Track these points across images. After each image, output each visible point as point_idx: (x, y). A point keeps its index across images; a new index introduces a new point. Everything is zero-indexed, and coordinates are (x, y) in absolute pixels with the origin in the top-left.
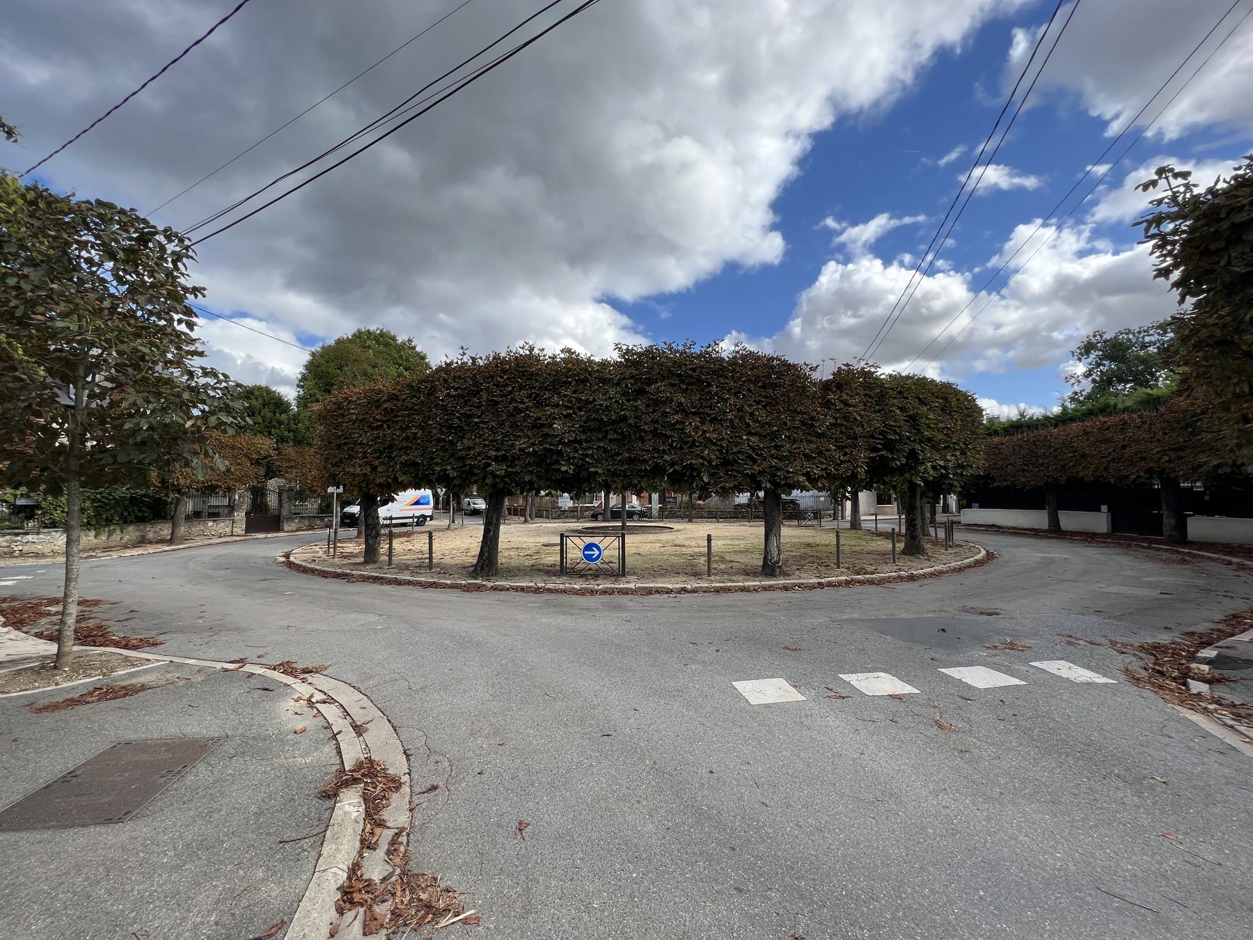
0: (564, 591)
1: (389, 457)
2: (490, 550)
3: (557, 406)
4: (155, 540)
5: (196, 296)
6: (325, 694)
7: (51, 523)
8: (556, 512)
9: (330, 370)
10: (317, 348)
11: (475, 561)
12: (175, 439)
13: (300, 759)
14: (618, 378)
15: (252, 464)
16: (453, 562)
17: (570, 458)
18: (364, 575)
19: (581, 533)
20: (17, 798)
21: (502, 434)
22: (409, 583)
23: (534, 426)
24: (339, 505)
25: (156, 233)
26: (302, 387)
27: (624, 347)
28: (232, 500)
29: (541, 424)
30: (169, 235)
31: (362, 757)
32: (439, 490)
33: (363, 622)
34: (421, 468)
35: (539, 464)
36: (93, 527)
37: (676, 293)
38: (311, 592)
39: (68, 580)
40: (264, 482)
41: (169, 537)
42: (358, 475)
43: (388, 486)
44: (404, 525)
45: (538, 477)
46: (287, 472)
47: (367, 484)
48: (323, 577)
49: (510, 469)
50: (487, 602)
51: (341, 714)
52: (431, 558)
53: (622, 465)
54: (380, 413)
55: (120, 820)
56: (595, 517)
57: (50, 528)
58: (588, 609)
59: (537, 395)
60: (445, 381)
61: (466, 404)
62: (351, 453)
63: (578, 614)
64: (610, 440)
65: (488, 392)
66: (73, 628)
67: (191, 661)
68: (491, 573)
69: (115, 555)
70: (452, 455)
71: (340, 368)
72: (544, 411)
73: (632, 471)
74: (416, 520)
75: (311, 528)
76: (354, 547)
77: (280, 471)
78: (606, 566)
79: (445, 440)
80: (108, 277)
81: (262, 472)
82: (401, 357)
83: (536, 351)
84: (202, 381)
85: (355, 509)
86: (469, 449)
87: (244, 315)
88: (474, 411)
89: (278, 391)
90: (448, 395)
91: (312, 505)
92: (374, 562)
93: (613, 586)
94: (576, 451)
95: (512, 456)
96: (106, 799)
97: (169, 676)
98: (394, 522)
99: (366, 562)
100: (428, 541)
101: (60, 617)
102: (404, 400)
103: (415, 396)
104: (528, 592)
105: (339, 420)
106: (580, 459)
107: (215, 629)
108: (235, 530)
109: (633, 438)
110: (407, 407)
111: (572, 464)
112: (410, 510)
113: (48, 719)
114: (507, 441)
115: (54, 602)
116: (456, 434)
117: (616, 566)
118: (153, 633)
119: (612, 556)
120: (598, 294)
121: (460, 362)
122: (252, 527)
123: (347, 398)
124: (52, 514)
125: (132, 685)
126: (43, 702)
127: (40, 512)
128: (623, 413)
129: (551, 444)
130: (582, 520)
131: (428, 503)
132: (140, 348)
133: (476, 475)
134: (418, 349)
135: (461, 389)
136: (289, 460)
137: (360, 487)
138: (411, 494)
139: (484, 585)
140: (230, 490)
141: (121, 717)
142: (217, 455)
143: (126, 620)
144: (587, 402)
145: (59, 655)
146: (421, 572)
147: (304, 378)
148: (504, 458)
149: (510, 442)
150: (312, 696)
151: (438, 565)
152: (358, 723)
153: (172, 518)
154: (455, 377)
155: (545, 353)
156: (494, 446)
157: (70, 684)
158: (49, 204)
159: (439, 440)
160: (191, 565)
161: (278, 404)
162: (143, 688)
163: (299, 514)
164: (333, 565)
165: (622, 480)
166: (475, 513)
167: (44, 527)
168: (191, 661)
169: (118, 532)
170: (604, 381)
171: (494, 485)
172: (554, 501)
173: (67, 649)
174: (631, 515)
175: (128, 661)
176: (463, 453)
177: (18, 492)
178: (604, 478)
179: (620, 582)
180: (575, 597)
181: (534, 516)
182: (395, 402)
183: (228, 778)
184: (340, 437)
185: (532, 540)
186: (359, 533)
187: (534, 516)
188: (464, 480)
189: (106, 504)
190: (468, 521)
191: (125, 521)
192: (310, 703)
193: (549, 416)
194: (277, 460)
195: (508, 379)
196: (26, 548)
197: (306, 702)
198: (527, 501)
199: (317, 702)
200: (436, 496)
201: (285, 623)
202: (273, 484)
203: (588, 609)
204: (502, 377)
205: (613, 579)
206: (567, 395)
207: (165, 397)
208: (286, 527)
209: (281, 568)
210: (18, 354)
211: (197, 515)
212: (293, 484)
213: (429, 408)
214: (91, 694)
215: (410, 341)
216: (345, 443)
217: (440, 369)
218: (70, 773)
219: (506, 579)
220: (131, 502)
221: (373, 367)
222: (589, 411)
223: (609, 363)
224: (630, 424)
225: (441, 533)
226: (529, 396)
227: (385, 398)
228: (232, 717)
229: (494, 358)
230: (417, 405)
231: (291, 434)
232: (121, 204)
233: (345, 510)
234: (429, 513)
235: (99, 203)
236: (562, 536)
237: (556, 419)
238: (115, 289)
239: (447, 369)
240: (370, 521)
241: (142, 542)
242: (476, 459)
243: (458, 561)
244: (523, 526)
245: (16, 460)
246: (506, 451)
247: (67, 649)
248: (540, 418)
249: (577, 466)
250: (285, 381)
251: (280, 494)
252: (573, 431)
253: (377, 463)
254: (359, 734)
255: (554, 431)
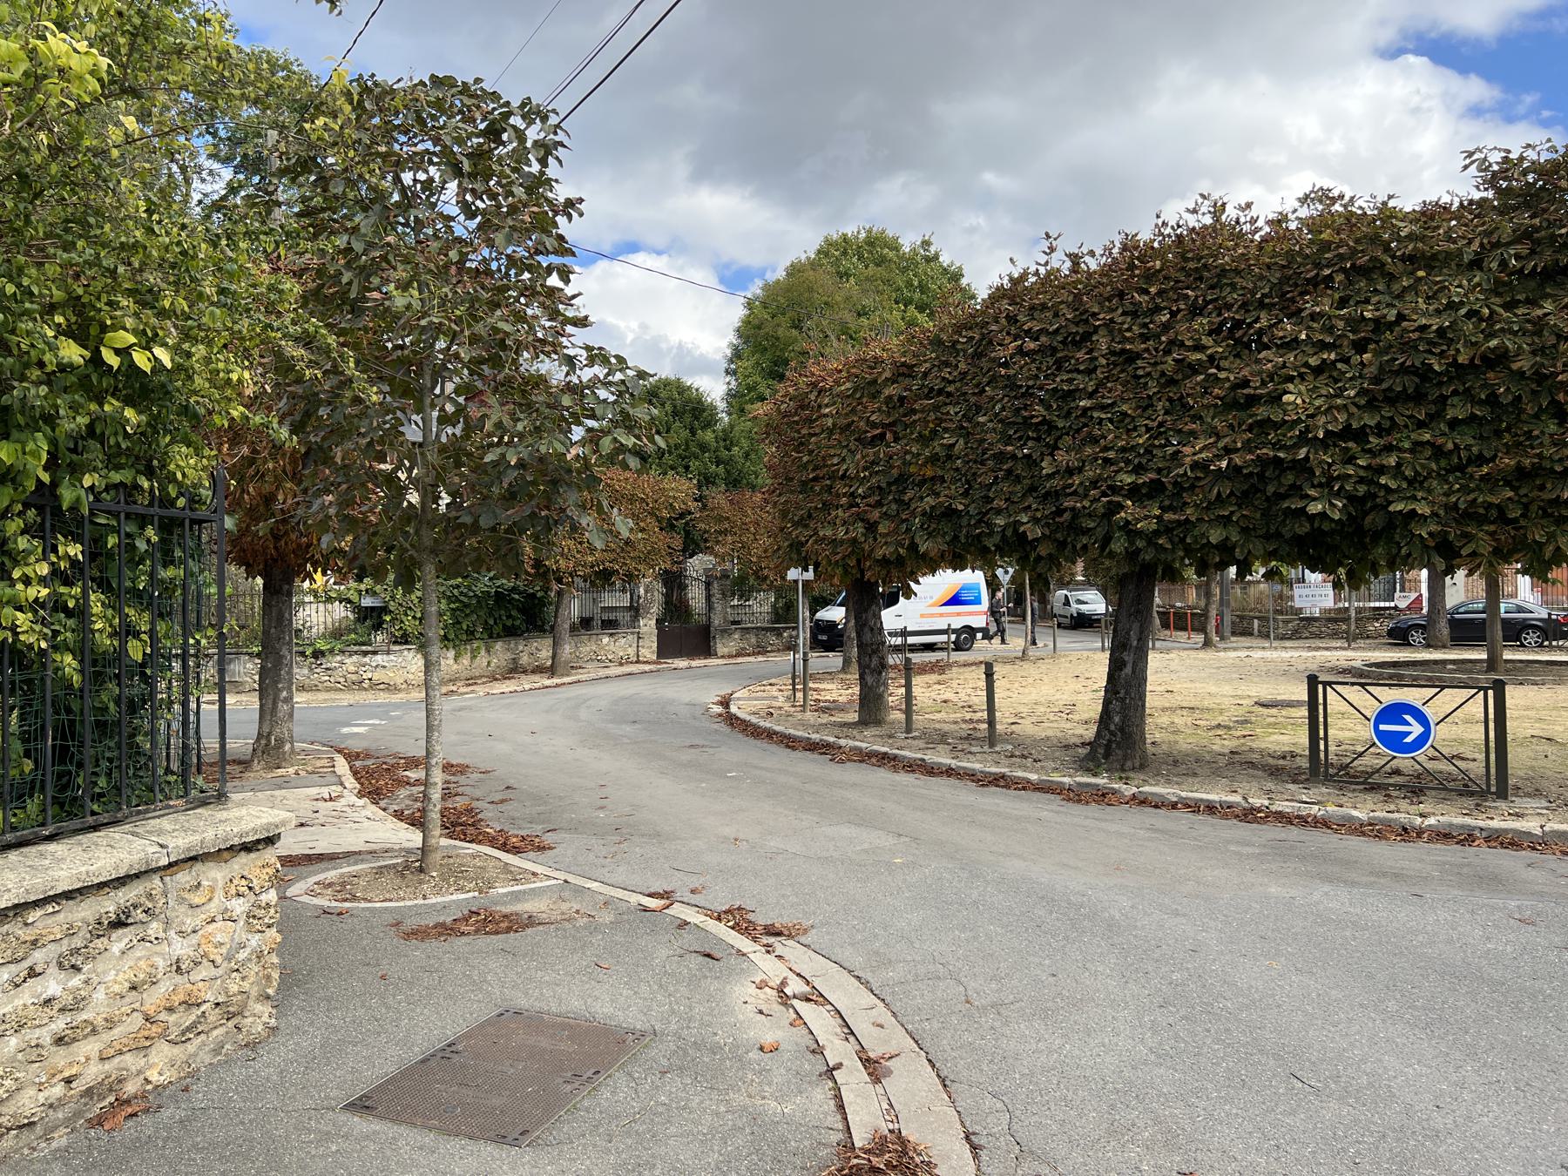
0: (1324, 823)
1: (899, 502)
2: (1124, 710)
3: (1292, 344)
4: (530, 668)
5: (570, 218)
6: (808, 983)
7: (402, 637)
8: (1286, 622)
9: (780, 332)
10: (755, 289)
11: (1090, 733)
12: (555, 483)
13: (773, 1104)
14: (1475, 246)
15: (661, 529)
16: (1040, 732)
17: (1331, 480)
18: (860, 749)
19: (1364, 677)
20: (391, 1069)
21: (1148, 430)
22: (949, 772)
23: (1230, 405)
24: (807, 606)
25: (510, 114)
26: (734, 373)
27: (1495, 157)
28: (635, 598)
29: (1248, 396)
30: (532, 112)
31: (884, 1128)
32: (999, 572)
33: (866, 846)
34: (964, 522)
35: (1244, 499)
36: (451, 644)
37: (1473, 76)
38: (769, 775)
39: (429, 728)
40: (680, 563)
41: (549, 663)
42: (842, 542)
43: (900, 562)
44: (930, 647)
45: (1245, 531)
46: (718, 542)
47: (859, 561)
48: (789, 747)
49: (1168, 516)
50: (1125, 829)
51: (838, 1030)
52: (991, 722)
53: (1491, 492)
54: (879, 410)
55: (515, 1143)
56: (1399, 636)
57: (400, 643)
58: (1398, 876)
59: (1237, 324)
60: (1012, 319)
61: (1058, 369)
62: (826, 496)
63: (1367, 886)
64: (1454, 424)
65: (1111, 332)
66: (439, 807)
67: (594, 885)
68: (1129, 764)
69: (481, 690)
70: (1032, 489)
71: (797, 325)
72: (1258, 361)
73: (1526, 507)
74: (953, 637)
75: (761, 650)
76: (841, 691)
77: (706, 541)
78: (1443, 766)
79: (1014, 457)
80: (453, 210)
81: (677, 543)
82: (909, 284)
83: (1231, 213)
84: (586, 374)
85: (836, 614)
86: (1070, 472)
87: (633, 248)
88: (1081, 381)
89: (695, 386)
90: (1020, 351)
91: (761, 605)
92: (878, 722)
93: (1468, 821)
94: (1350, 460)
95: (1175, 484)
96: (496, 1101)
97: (564, 906)
98: (911, 640)
99: (863, 723)
100: (982, 684)
101: (422, 788)
102: (925, 374)
103: (947, 364)
104: (1225, 817)
105: (804, 431)
106: (1361, 480)
107: (624, 831)
108: (642, 651)
109: (1530, 409)
110: (932, 389)
111: (1338, 494)
112: (941, 615)
113: (418, 951)
114: (1162, 446)
115: (413, 763)
116: (1038, 439)
117: (1477, 769)
118: (538, 829)
119: (1462, 742)
120: (1387, 35)
121: (1042, 270)
122: (668, 647)
123: (814, 385)
124: (402, 622)
125: (517, 914)
126: (411, 923)
127: (388, 618)
128: (1494, 343)
129: (1277, 446)
130: (1361, 643)
131: (977, 601)
132: (501, 325)
133: (1087, 532)
134: (945, 259)
135: (1048, 333)
136: (720, 519)
137: (845, 568)
138: (946, 580)
139: (1115, 792)
140: (631, 578)
141: (506, 967)
142: (615, 510)
143: (502, 801)
144: (1379, 324)
145: (425, 849)
146: (974, 749)
147: (737, 355)
148: (1156, 488)
149: (1170, 450)
150: (784, 983)
151: (1009, 737)
152: (872, 1055)
153: (553, 627)
154: (1032, 308)
155: (1253, 213)
156: (1128, 462)
157: (440, 899)
158: (378, 99)
159: (1001, 457)
160: (583, 714)
161: (690, 409)
162: (532, 921)
163: (738, 623)
164: (804, 725)
165: (1492, 534)
166: (1083, 623)
167: (395, 643)
168: (594, 885)
169: (483, 652)
170: (1432, 262)
171: (1132, 555)
172: (1281, 597)
173: (433, 841)
174: (1516, 631)
175: (515, 876)
176: (1056, 483)
177: (363, 587)
178: (1433, 528)
179: (1491, 813)
180: (1355, 842)
181: (1227, 633)
182: (907, 381)
183: (660, 1109)
184: (805, 466)
185: (1227, 689)
186: (847, 663)
187: (1227, 633)
188: (1062, 545)
189: (466, 606)
190: (1070, 642)
191: (491, 636)
192: (784, 998)
193: (1271, 376)
194: (701, 519)
195: (1160, 293)
196: (377, 676)
197: (775, 993)
198: (1208, 595)
199: (795, 997)
200: (993, 585)
201: (729, 831)
202: (698, 565)
203: (1398, 876)
204: (1146, 292)
205: (1470, 802)
206: (1321, 314)
207: (537, 410)
208: (721, 649)
209: (716, 726)
210: (349, 368)
211: (586, 623)
212: (728, 565)
213: (977, 386)
214: (466, 919)
215: (926, 244)
216: (815, 479)
217: (998, 295)
218: (449, 1046)
219: (1168, 782)
220: (496, 601)
221: (859, 315)
222: (1386, 351)
223: (1446, 209)
224: (1521, 373)
225: (1008, 667)
226: (1214, 331)
227: (887, 374)
228: (659, 997)
229: (1124, 248)
230: (953, 382)
231: (721, 469)
232: (464, 76)
233: (819, 615)
234: (979, 622)
235: (435, 79)
236: (1313, 681)
237: (1291, 379)
238: (463, 227)
239: (1012, 293)
240: (868, 637)
241: (514, 670)
242: (1086, 496)
243: (1049, 730)
244: (1202, 654)
245: (360, 531)
246: (1159, 471)
247: (433, 841)
248: (1245, 383)
249: (1351, 499)
250: (704, 367)
251: (708, 585)
252: (1338, 408)
253: (875, 515)
254: (877, 1080)
255: (1285, 412)
